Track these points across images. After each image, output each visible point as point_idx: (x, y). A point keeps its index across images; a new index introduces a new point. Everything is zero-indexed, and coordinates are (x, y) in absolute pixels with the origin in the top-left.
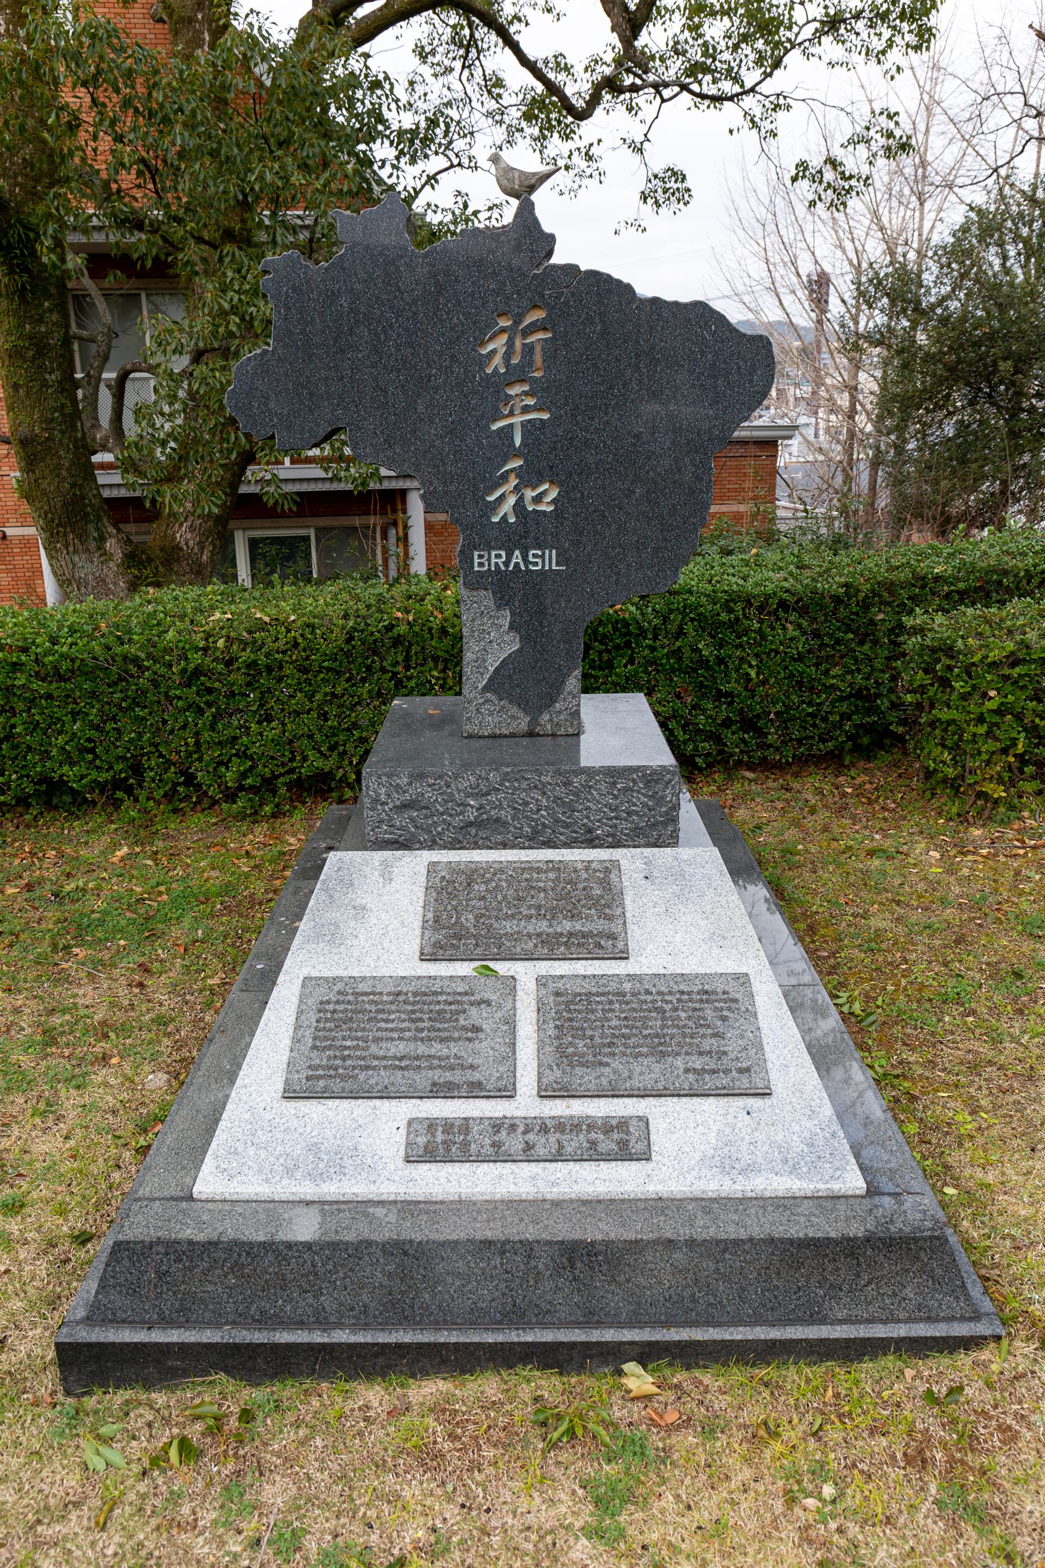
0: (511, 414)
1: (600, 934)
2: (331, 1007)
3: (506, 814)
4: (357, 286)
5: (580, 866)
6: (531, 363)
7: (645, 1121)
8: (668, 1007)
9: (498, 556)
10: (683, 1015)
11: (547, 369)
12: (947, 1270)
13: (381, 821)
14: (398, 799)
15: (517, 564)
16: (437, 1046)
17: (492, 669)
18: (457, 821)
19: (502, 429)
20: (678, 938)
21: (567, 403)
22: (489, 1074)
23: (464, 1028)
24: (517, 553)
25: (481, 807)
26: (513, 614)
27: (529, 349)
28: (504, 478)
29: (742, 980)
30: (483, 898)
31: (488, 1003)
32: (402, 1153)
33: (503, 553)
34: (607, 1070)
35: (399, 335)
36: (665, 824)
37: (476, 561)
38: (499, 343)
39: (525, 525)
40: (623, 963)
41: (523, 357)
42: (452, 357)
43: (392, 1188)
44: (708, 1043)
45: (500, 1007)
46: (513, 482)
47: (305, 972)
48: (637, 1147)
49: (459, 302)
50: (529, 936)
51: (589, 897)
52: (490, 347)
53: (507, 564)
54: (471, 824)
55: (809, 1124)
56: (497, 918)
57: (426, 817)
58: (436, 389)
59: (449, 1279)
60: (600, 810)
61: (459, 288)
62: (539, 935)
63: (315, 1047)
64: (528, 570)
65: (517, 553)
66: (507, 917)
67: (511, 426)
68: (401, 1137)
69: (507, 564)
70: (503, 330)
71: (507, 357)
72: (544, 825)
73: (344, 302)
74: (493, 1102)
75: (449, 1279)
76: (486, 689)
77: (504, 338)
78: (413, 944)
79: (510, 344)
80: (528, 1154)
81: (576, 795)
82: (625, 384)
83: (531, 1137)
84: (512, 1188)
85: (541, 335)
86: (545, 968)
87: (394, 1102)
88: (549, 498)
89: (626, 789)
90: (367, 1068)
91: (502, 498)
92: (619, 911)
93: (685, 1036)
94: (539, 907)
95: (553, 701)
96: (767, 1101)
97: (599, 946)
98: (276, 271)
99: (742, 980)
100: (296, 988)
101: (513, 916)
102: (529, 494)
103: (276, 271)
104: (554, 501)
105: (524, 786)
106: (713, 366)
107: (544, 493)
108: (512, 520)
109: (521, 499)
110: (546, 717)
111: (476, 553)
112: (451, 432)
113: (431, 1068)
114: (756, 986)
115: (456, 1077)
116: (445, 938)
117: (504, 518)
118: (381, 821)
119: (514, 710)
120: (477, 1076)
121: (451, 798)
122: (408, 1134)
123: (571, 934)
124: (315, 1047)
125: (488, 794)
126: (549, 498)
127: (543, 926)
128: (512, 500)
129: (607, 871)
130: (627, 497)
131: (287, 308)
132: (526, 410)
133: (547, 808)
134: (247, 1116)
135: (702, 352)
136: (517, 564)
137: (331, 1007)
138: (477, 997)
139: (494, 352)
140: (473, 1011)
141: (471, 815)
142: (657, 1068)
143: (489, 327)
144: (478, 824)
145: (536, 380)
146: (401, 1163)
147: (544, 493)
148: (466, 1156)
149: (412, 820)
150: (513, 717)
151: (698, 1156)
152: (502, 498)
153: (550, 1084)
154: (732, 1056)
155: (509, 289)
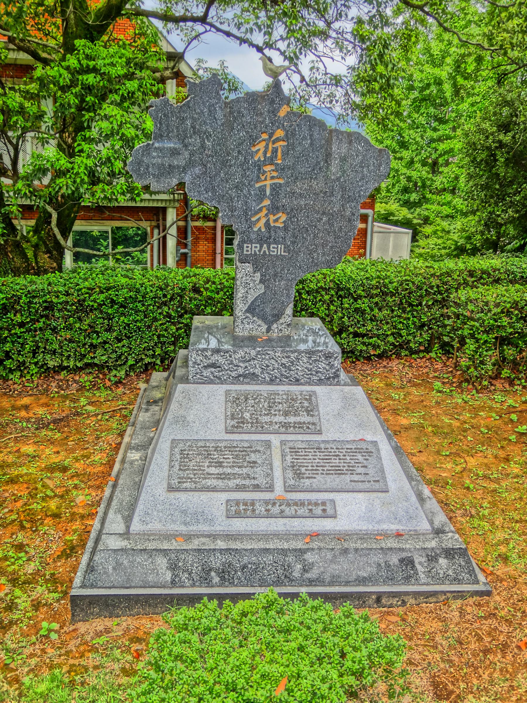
0: (266, 179)
1: (309, 423)
2: (186, 452)
3: (258, 371)
4: (195, 116)
5: (297, 393)
6: (276, 157)
7: (333, 502)
8: (341, 454)
9: (256, 247)
10: (348, 458)
11: (284, 159)
12: (467, 563)
13: (197, 373)
14: (206, 362)
15: (265, 252)
16: (237, 469)
17: (250, 302)
18: (234, 374)
19: (261, 187)
20: (344, 425)
21: (292, 176)
22: (262, 481)
23: (249, 462)
24: (265, 245)
25: (246, 367)
26: (262, 275)
27: (275, 151)
28: (261, 210)
29: (375, 443)
30: (253, 406)
31: (259, 451)
32: (225, 514)
33: (258, 245)
34: (314, 480)
35: (214, 140)
36: (334, 378)
37: (245, 249)
38: (261, 146)
39: (270, 232)
40: (320, 436)
41: (273, 153)
42: (239, 152)
43: (222, 528)
44: (360, 470)
45: (264, 453)
46: (265, 211)
47: (172, 437)
48: (330, 512)
49: (243, 126)
50: (276, 423)
51: (302, 407)
52: (257, 148)
53: (260, 251)
54: (240, 376)
55: (406, 504)
56: (261, 415)
57: (219, 371)
58: (230, 166)
59: (250, 566)
60: (303, 370)
61: (244, 119)
62: (280, 423)
63: (180, 469)
64: (270, 255)
65: (265, 245)
66: (265, 415)
67: (265, 185)
68: (223, 508)
69: (260, 251)
70: (264, 140)
71: (265, 153)
72: (276, 377)
73: (189, 123)
74: (264, 493)
75: (250, 566)
76: (247, 311)
77: (264, 144)
78: (221, 427)
79: (267, 147)
80: (282, 515)
81: (292, 362)
82: (320, 169)
83: (283, 507)
84: (275, 528)
85: (282, 143)
86: (284, 437)
87: (219, 493)
88: (281, 220)
89: (316, 360)
90: (206, 478)
91: (259, 219)
92: (317, 413)
93: (351, 464)
94: (280, 411)
95: (279, 319)
96: (387, 494)
97: (308, 428)
98: (156, 106)
99: (375, 443)
100: (168, 444)
101: (268, 414)
102: (272, 218)
103: (156, 106)
104: (284, 222)
105: (267, 357)
106: (362, 162)
107: (279, 218)
108: (263, 230)
109: (268, 220)
110: (275, 326)
111: (245, 245)
112: (236, 187)
113: (235, 478)
114: (381, 446)
115: (247, 482)
116: (237, 423)
117: (260, 229)
118: (197, 373)
119: (260, 322)
120: (256, 482)
121: (232, 363)
122: (227, 506)
123: (295, 423)
124: (180, 469)
125: (250, 361)
126: (281, 220)
127: (282, 419)
128: (263, 221)
129: (310, 396)
130: (319, 221)
131: (161, 124)
132: (272, 178)
133: (278, 369)
134: (152, 499)
135: (357, 156)
136: (265, 252)
137: (186, 452)
138: (254, 449)
139: (259, 150)
140: (252, 455)
141: (241, 371)
142: (338, 480)
143: (257, 138)
144: (245, 376)
145: (277, 164)
146: (224, 518)
147: (279, 218)
148: (255, 515)
149: (212, 373)
150: (259, 326)
151: (357, 516)
152: (259, 219)
153: (289, 486)
154: (371, 475)
155: (267, 121)
